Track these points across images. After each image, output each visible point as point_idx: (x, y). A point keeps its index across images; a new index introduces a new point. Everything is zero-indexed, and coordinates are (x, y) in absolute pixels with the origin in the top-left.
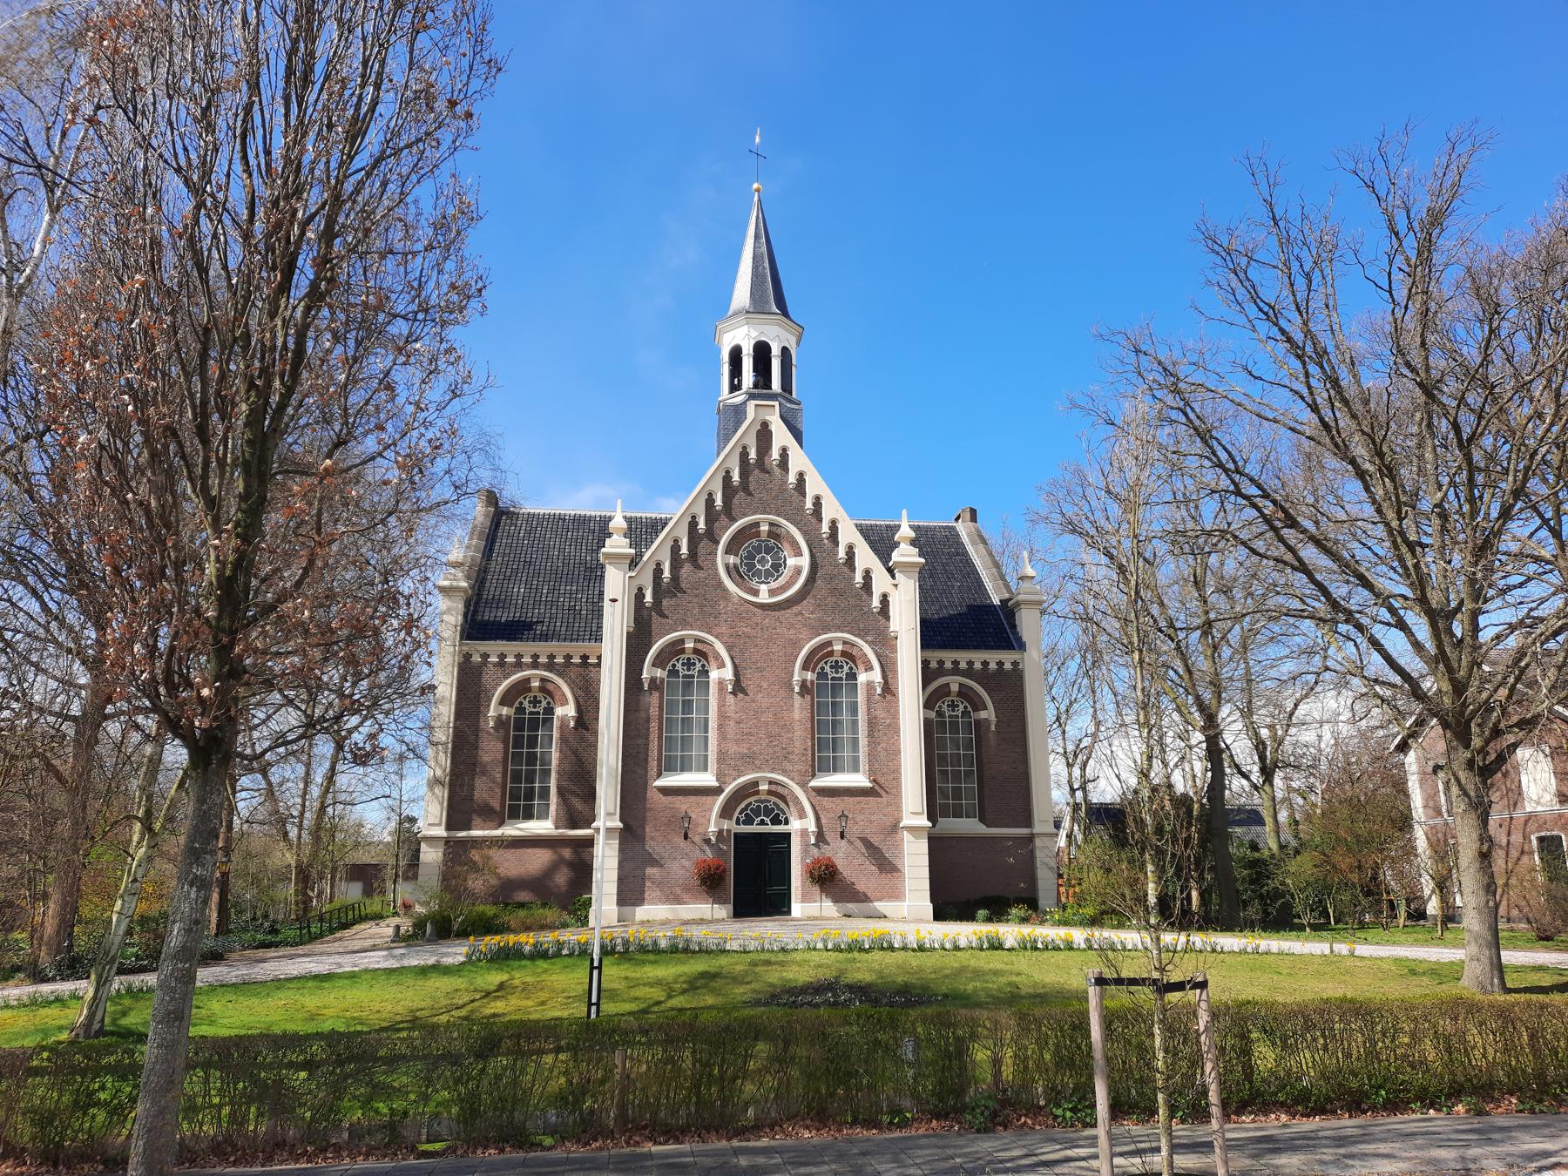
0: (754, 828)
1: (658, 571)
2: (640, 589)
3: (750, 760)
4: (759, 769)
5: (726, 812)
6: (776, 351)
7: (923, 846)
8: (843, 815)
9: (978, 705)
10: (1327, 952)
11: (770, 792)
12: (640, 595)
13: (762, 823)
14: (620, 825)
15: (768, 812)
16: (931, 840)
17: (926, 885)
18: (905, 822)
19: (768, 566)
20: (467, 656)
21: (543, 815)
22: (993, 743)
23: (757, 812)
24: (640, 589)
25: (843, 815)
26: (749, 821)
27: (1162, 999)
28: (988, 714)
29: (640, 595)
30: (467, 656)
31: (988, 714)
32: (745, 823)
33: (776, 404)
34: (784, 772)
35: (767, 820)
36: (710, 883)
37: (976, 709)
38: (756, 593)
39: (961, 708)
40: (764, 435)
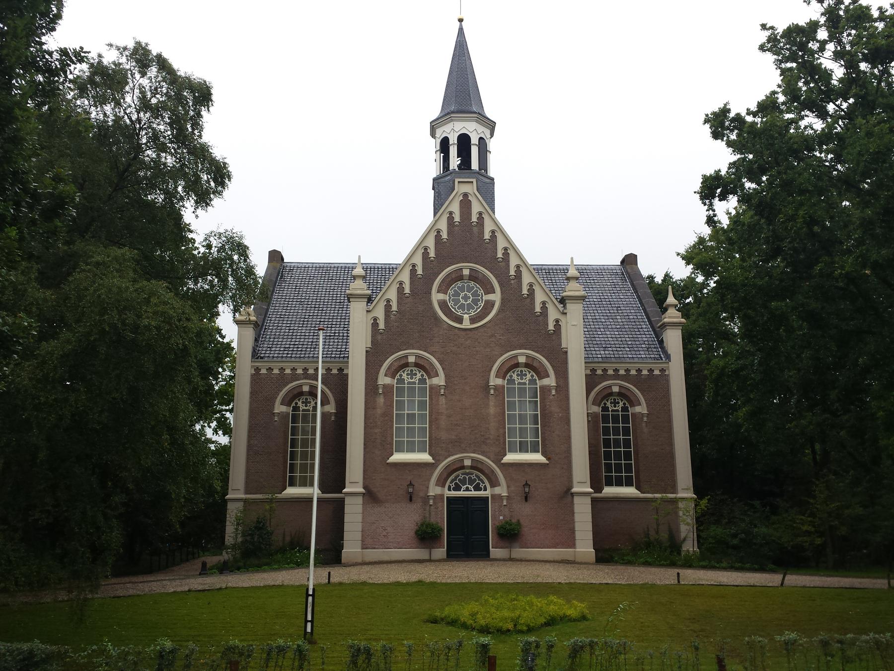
0: (462, 493)
1: (388, 306)
2: (375, 319)
3: (457, 445)
4: (465, 451)
5: (441, 482)
6: (474, 140)
7: (588, 508)
8: (527, 484)
9: (634, 402)
10: (886, 587)
11: (472, 467)
12: (375, 324)
13: (467, 489)
14: (362, 490)
15: (471, 482)
16: (594, 501)
17: (590, 536)
18: (575, 490)
19: (462, 294)
20: (257, 369)
21: (307, 482)
22: (646, 430)
23: (463, 482)
24: (375, 319)
25: (527, 484)
26: (458, 488)
27: (227, 548)
28: (641, 409)
29: (375, 324)
30: (257, 369)
31: (550, 381)
32: (454, 489)
33: (474, 180)
34: (483, 453)
35: (471, 487)
36: (426, 536)
37: (632, 405)
38: (460, 320)
39: (621, 404)
40: (466, 204)
